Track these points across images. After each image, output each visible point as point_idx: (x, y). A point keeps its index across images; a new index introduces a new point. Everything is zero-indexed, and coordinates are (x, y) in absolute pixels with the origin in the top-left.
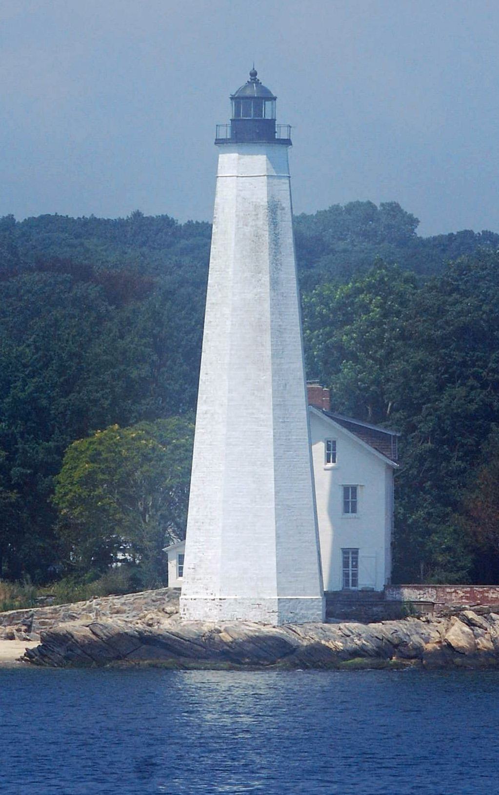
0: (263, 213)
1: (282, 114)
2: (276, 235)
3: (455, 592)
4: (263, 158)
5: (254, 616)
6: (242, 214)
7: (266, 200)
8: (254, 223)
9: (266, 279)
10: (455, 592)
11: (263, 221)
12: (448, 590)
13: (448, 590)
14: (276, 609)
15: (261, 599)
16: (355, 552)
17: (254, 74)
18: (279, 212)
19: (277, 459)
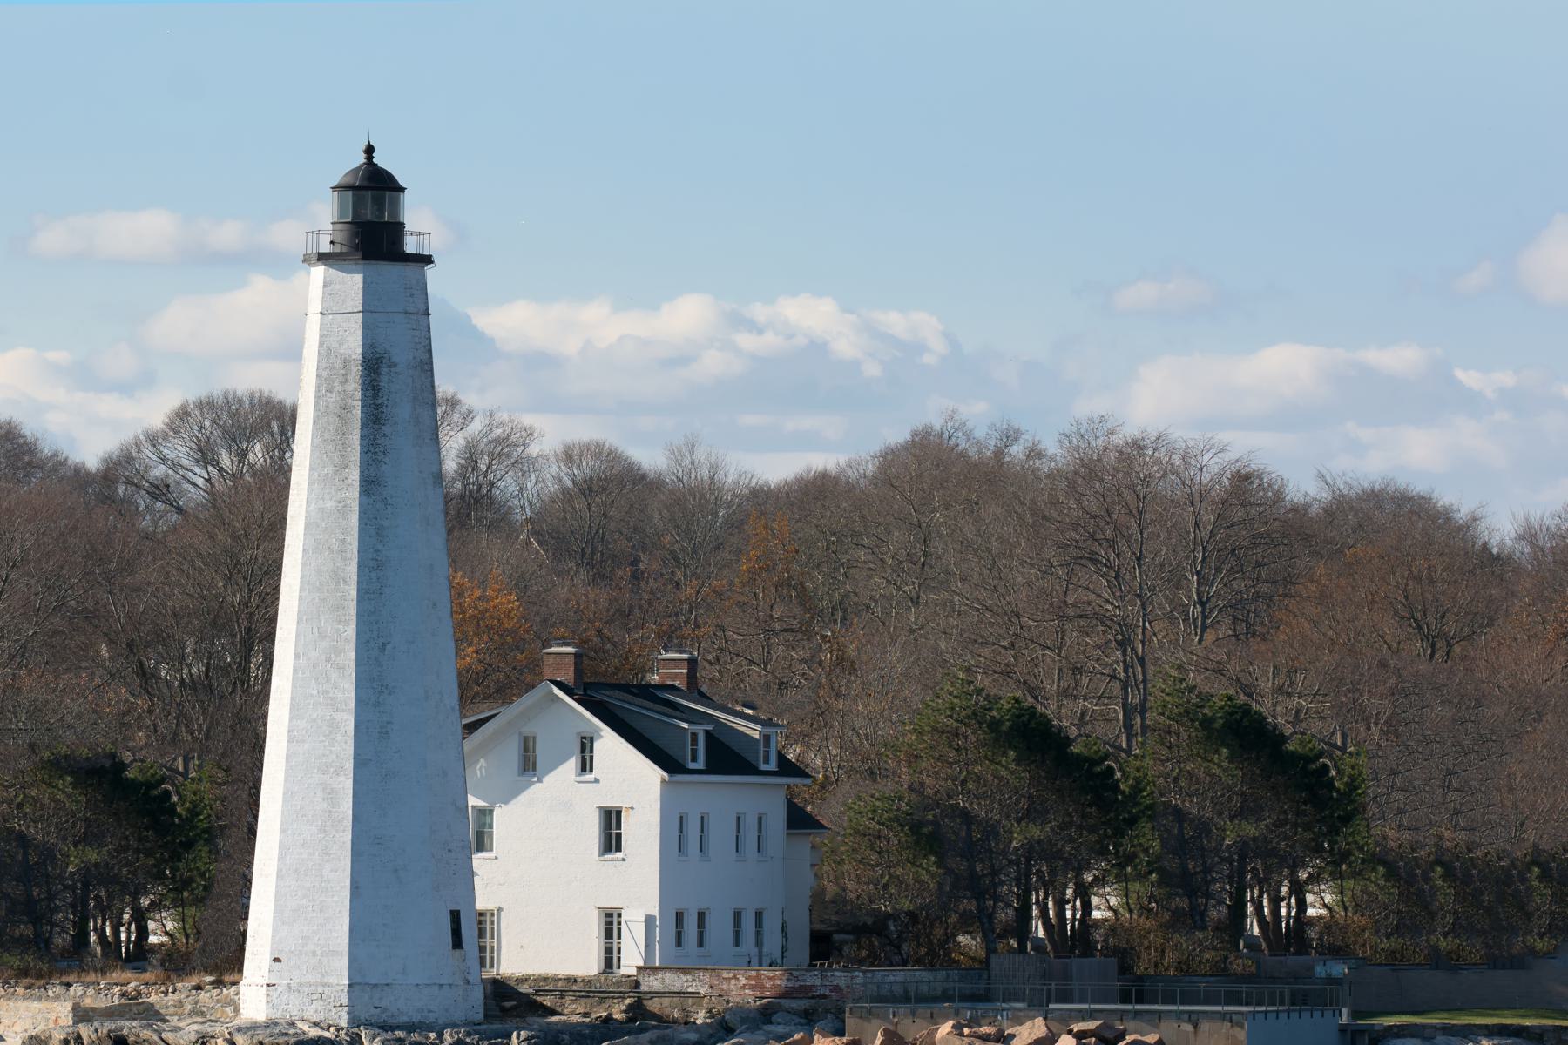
0: (356, 370)
1: (420, 221)
2: (378, 407)
3: (735, 977)
4: (357, 280)
5: (315, 1011)
6: (324, 374)
7: (359, 351)
8: (340, 388)
9: (354, 476)
10: (735, 977)
11: (354, 386)
12: (725, 975)
13: (725, 975)
14: (345, 1001)
15: (324, 985)
16: (458, 912)
17: (370, 150)
18: (384, 370)
19: (360, 763)
